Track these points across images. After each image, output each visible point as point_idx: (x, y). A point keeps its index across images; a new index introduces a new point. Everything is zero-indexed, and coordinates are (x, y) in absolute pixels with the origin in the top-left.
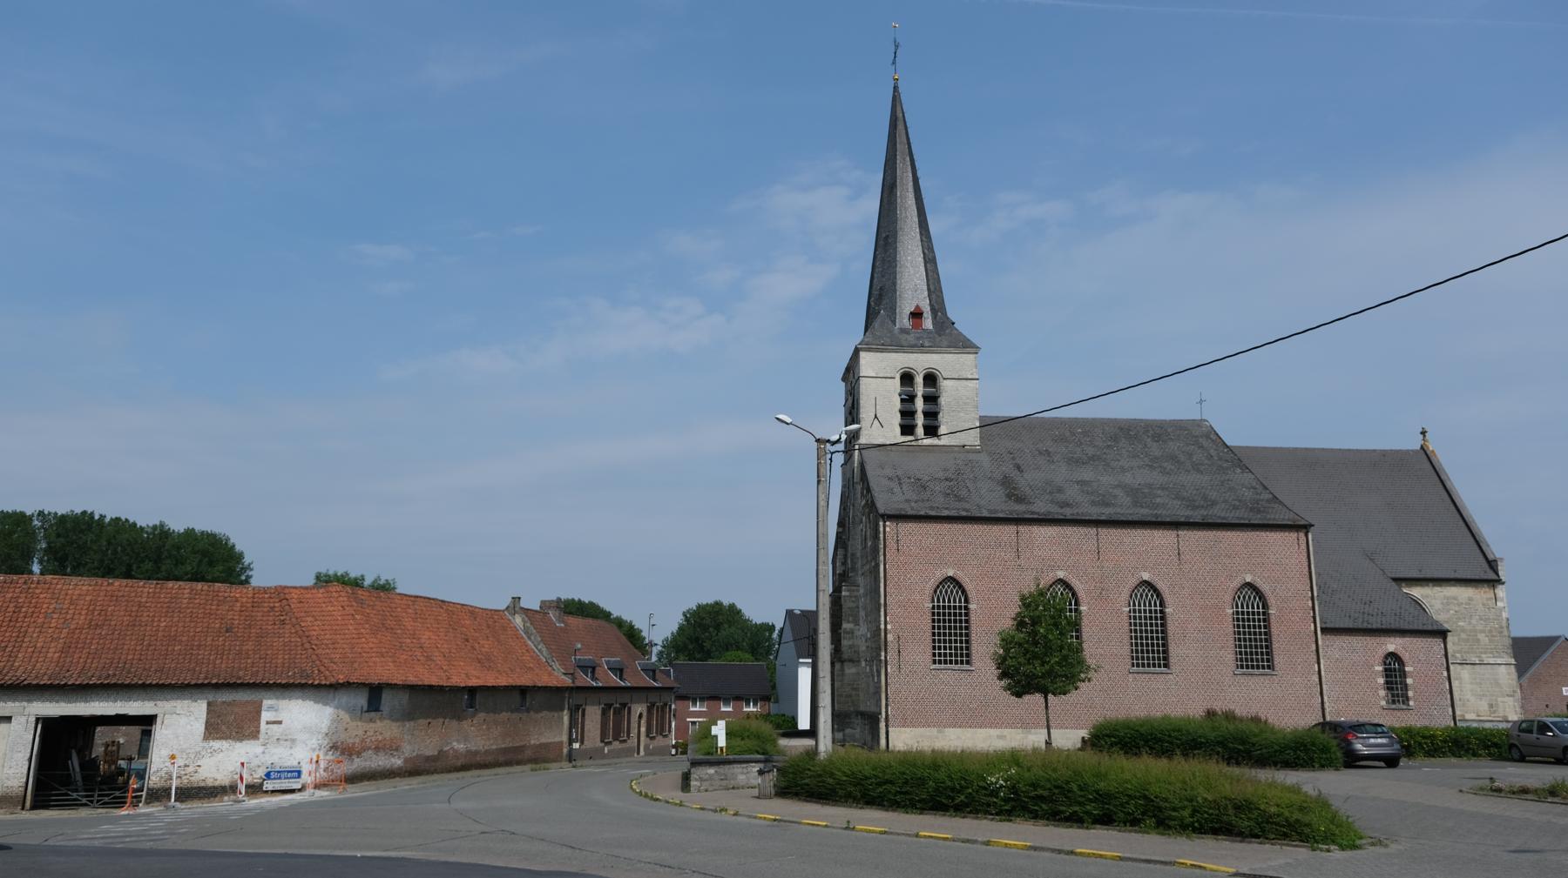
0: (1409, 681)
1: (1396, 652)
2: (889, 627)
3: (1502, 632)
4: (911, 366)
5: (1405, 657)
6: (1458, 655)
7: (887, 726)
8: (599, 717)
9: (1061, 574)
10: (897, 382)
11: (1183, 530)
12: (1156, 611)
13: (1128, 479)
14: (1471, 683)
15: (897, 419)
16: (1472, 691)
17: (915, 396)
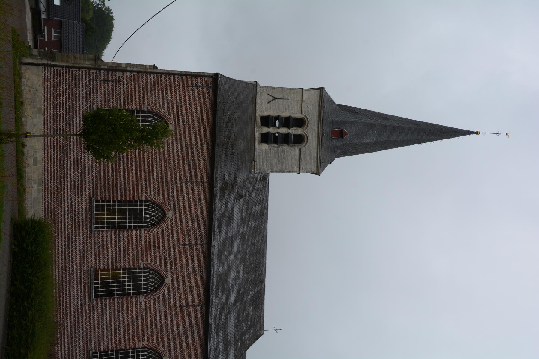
4: (309, 126)
7: (44, 65)
8: (28, 203)
9: (170, 215)
10: (298, 115)
12: (140, 289)
13: (233, 275)
15: (273, 114)
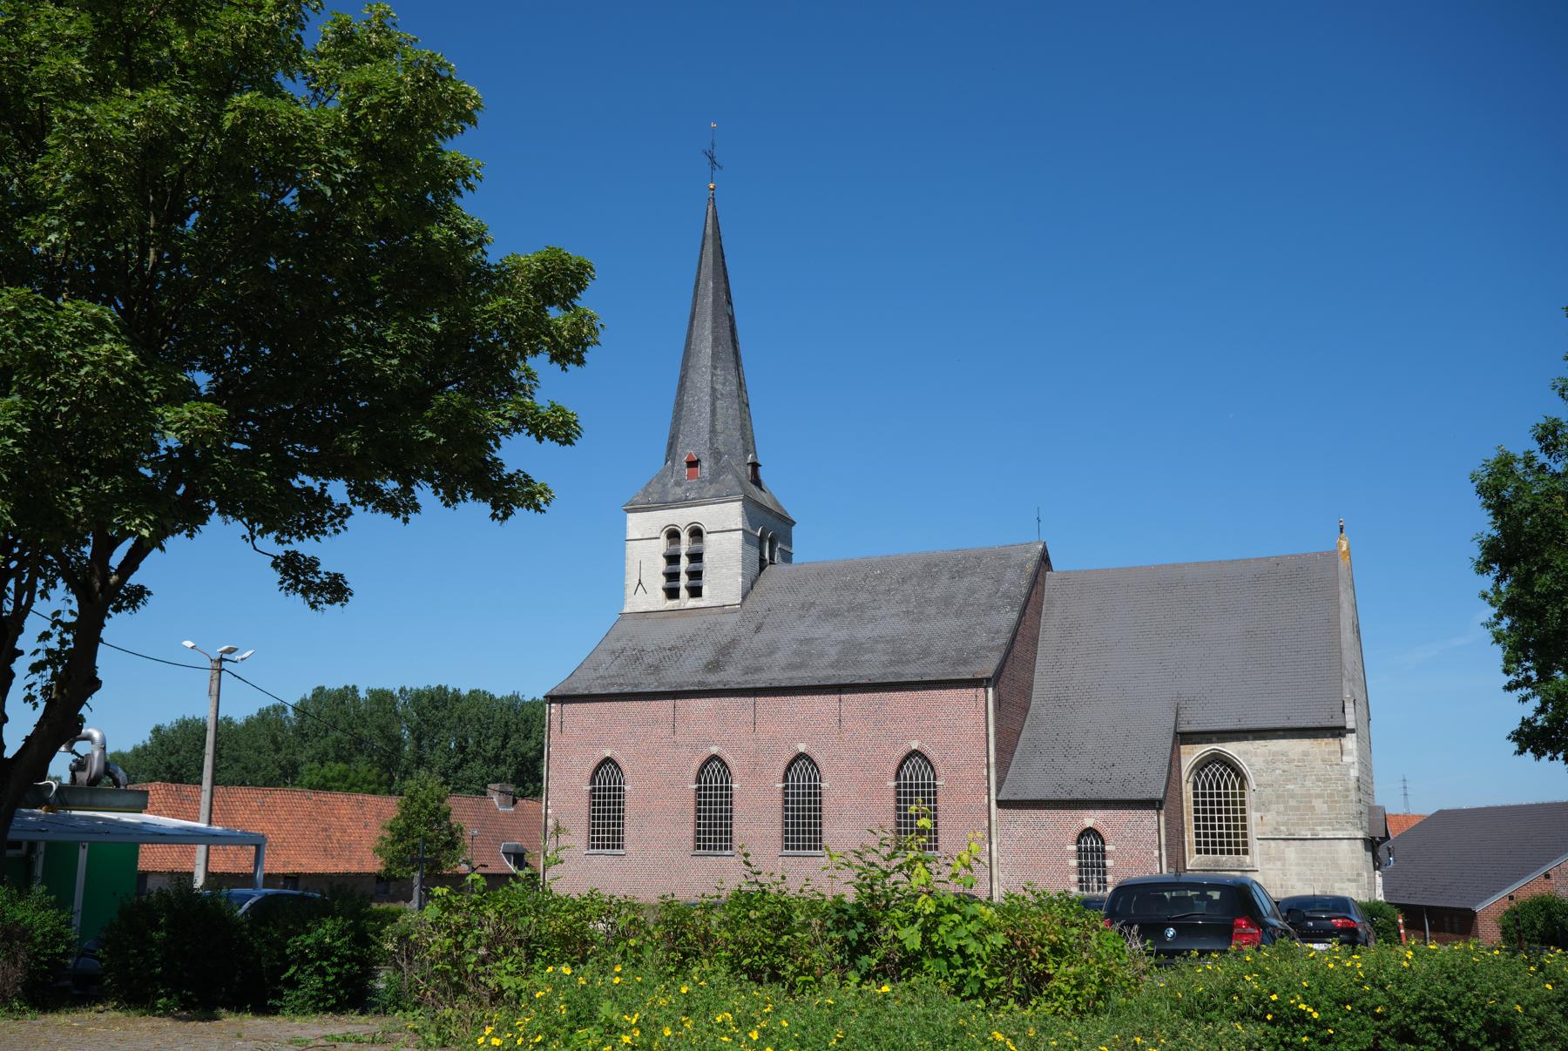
0: (1109, 863)
1: (1095, 827)
2: (549, 811)
3: (1347, 796)
5: (1106, 833)
6: (1282, 828)
11: (846, 693)
14: (1299, 864)
15: (662, 581)
16: (1298, 874)
17: (679, 556)
